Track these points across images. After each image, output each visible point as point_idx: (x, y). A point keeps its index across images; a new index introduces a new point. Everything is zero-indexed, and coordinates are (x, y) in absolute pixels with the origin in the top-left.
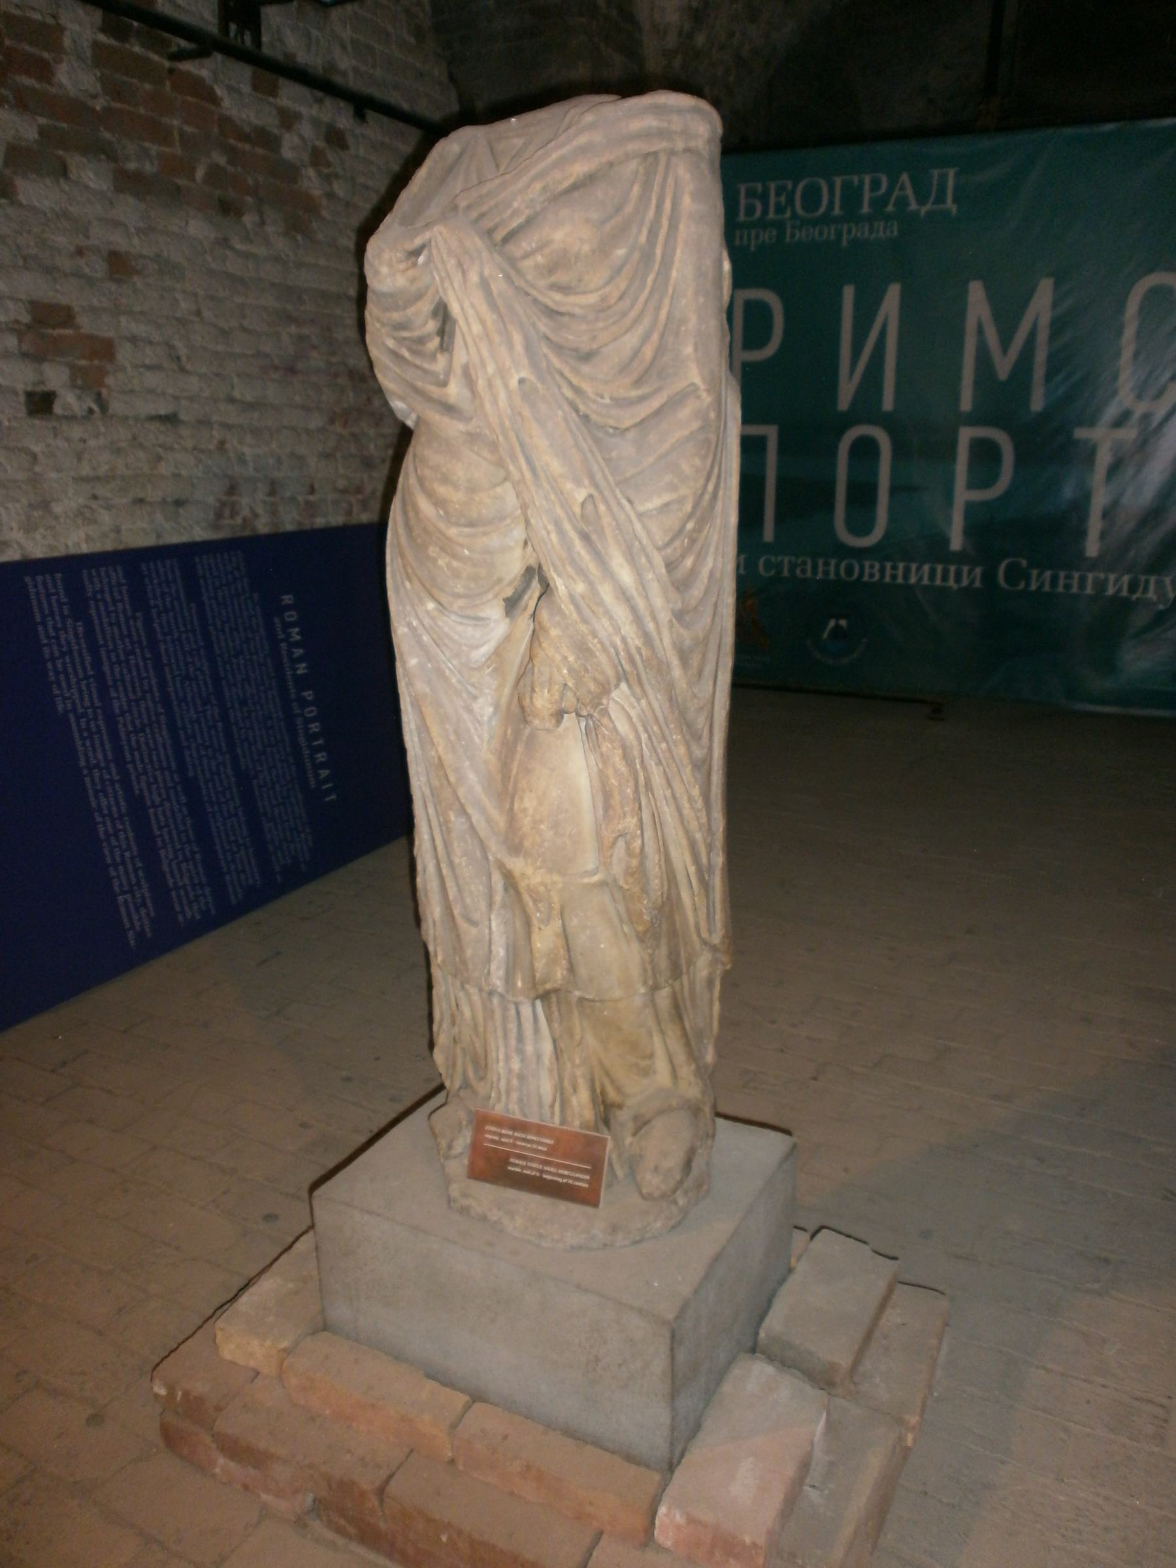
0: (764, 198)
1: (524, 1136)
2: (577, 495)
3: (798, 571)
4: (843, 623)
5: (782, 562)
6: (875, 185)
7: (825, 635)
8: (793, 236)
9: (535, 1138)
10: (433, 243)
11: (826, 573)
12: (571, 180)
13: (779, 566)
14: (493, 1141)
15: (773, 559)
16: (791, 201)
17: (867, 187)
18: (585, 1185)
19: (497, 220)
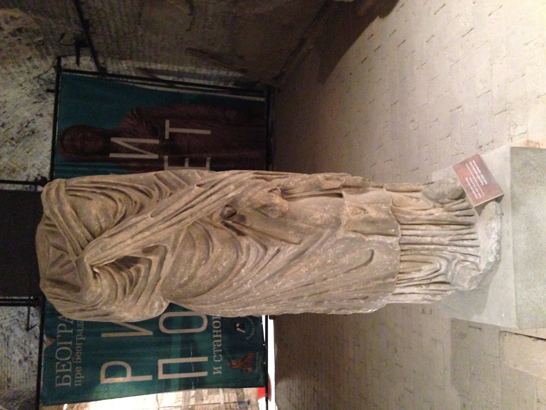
0: (62, 374)
1: (471, 187)
2: (197, 189)
3: (219, 346)
4: (238, 325)
5: (215, 352)
6: (62, 328)
7: (244, 332)
8: (78, 360)
9: (469, 183)
10: (91, 264)
11: (219, 334)
12: (72, 211)
13: (217, 354)
14: (481, 193)
15: (215, 356)
16: (63, 362)
17: (62, 331)
18: (474, 161)
19: (85, 239)
